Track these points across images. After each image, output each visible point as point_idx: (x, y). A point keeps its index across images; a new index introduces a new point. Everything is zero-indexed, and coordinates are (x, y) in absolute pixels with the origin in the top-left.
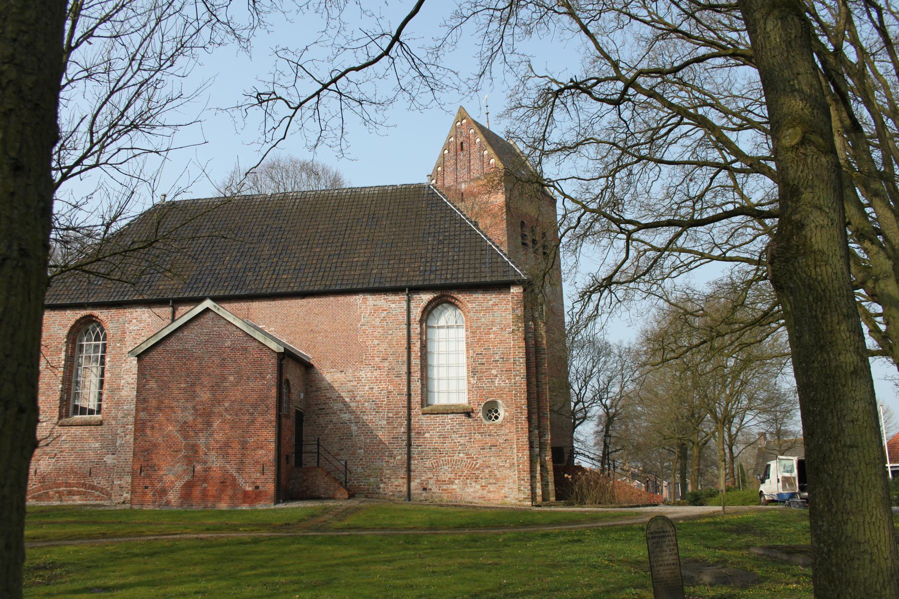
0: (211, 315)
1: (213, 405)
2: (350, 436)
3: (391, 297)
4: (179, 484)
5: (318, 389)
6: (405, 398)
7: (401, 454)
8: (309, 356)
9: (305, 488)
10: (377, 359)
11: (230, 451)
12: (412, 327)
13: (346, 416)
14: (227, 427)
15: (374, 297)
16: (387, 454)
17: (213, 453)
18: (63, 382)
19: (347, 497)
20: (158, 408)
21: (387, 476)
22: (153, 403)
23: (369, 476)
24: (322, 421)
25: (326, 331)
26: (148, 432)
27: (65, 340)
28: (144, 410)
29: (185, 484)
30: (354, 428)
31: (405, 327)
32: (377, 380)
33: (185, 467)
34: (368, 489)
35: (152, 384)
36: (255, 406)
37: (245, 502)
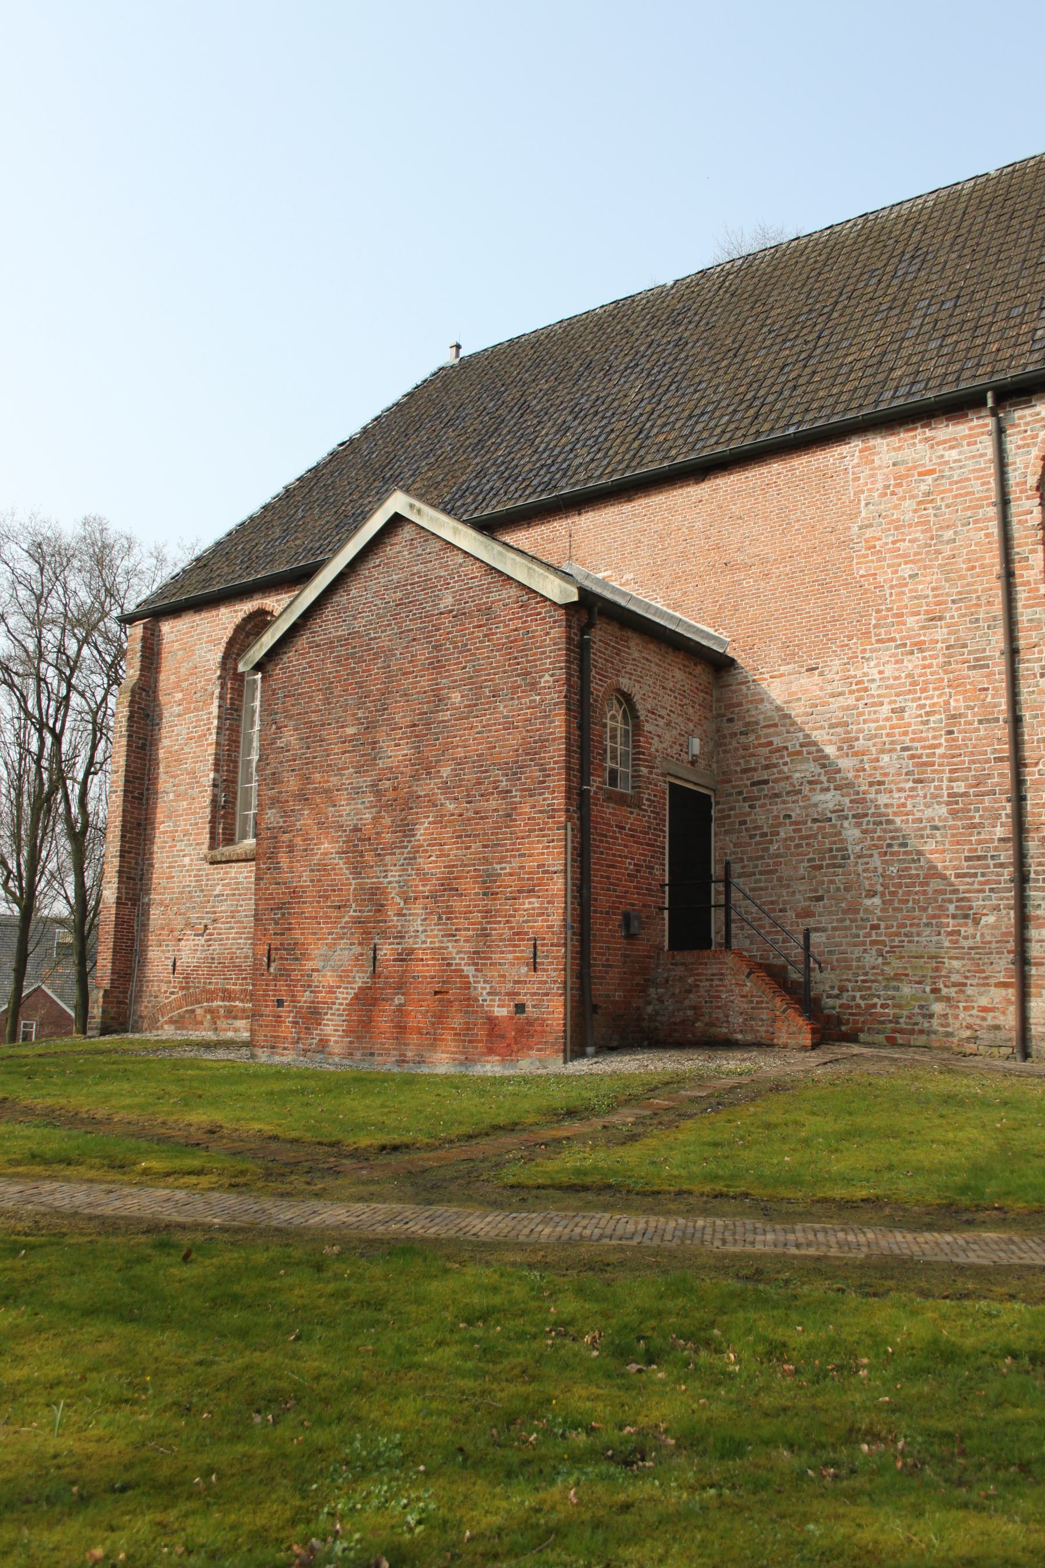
0: (406, 533)
1: (416, 777)
2: (839, 856)
3: (946, 431)
4: (344, 996)
5: (750, 728)
6: (1003, 731)
7: (996, 908)
8: (724, 635)
9: (689, 1013)
10: (911, 621)
11: (457, 904)
12: (1014, 508)
13: (828, 800)
14: (448, 833)
15: (893, 440)
16: (952, 908)
17: (418, 909)
18: (217, 766)
19: (808, 1042)
20: (303, 797)
21: (955, 978)
22: (292, 783)
23: (897, 977)
24: (761, 818)
25: (764, 561)
26: (284, 860)
27: (218, 673)
28: (275, 802)
29: (356, 997)
30: (851, 833)
31: (992, 511)
32: (914, 684)
33: (357, 949)
34: (896, 1019)
35: (289, 737)
36: (514, 771)
37: (491, 1051)
